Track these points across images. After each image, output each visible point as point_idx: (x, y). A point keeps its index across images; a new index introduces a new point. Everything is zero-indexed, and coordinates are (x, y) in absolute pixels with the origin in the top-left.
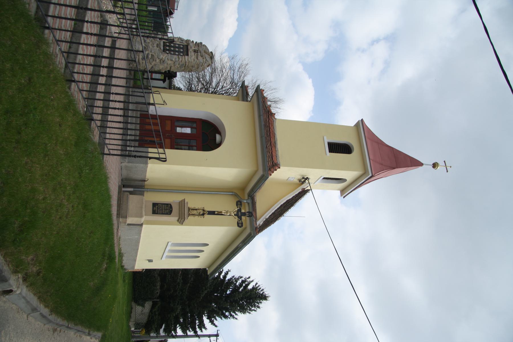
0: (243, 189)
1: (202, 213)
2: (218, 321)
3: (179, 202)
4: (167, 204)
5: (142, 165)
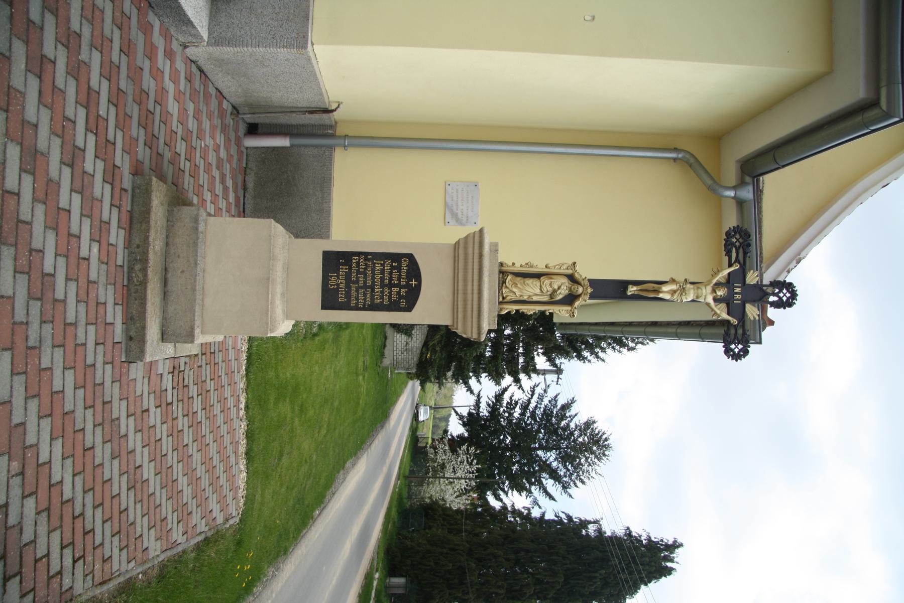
0: (717, 136)
1: (563, 293)
2: (569, 365)
3: (457, 245)
4: (396, 258)
5: (282, 53)
